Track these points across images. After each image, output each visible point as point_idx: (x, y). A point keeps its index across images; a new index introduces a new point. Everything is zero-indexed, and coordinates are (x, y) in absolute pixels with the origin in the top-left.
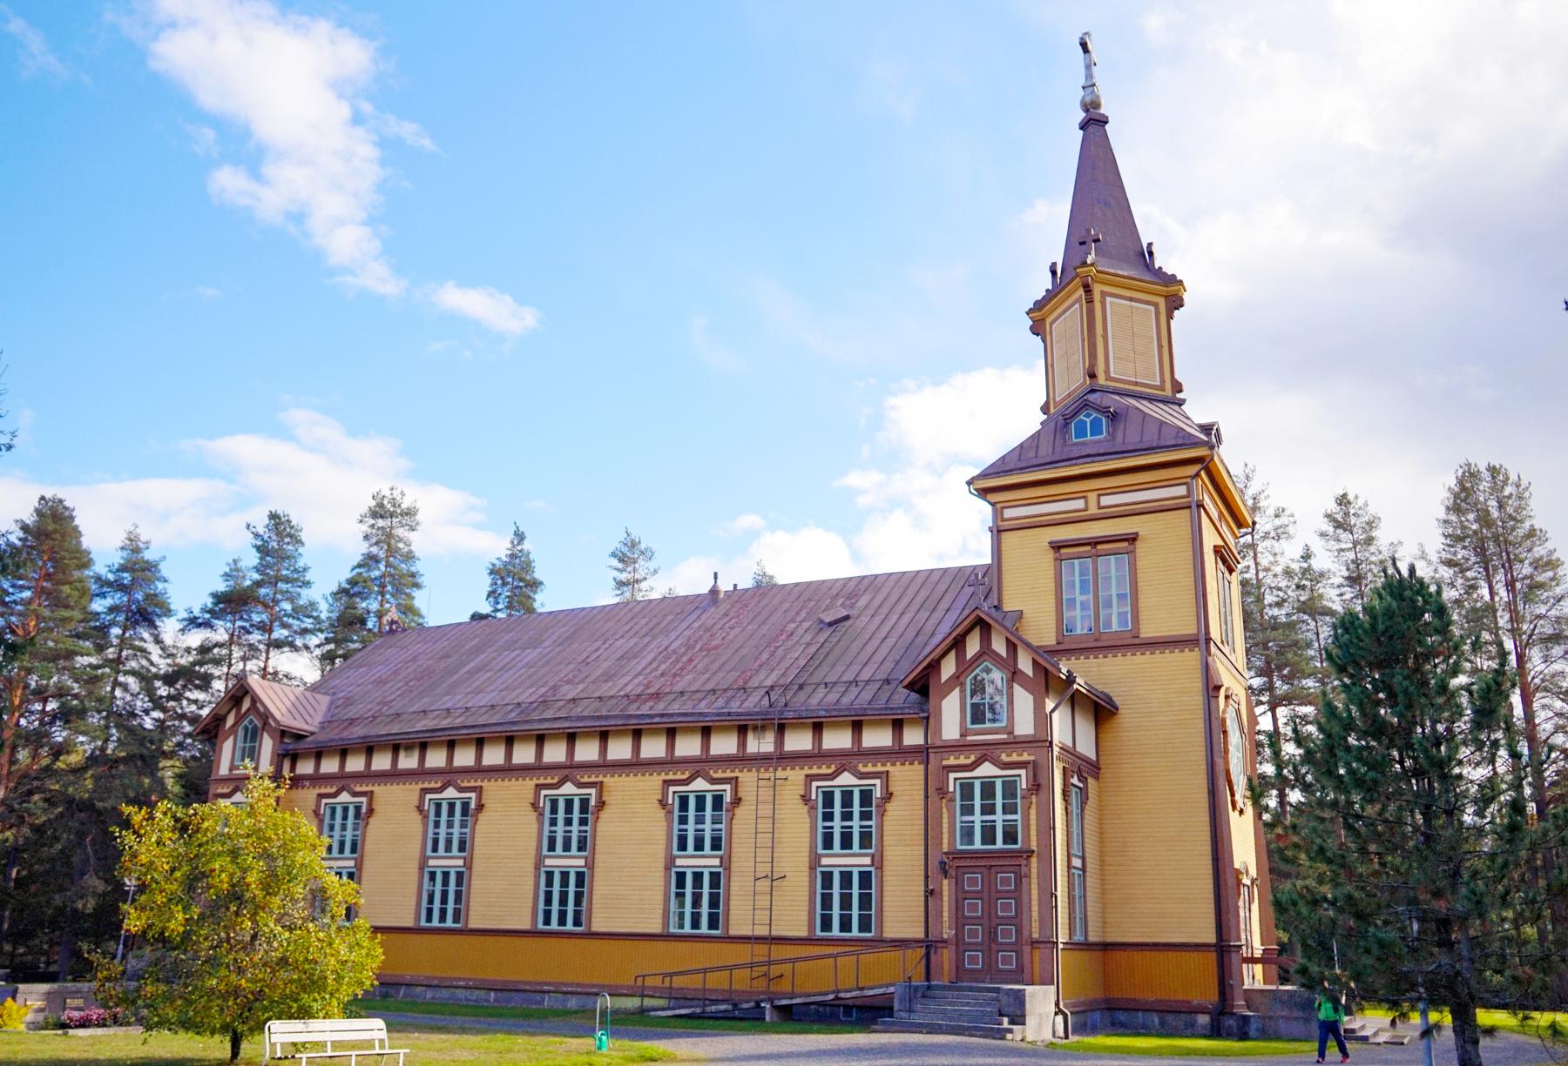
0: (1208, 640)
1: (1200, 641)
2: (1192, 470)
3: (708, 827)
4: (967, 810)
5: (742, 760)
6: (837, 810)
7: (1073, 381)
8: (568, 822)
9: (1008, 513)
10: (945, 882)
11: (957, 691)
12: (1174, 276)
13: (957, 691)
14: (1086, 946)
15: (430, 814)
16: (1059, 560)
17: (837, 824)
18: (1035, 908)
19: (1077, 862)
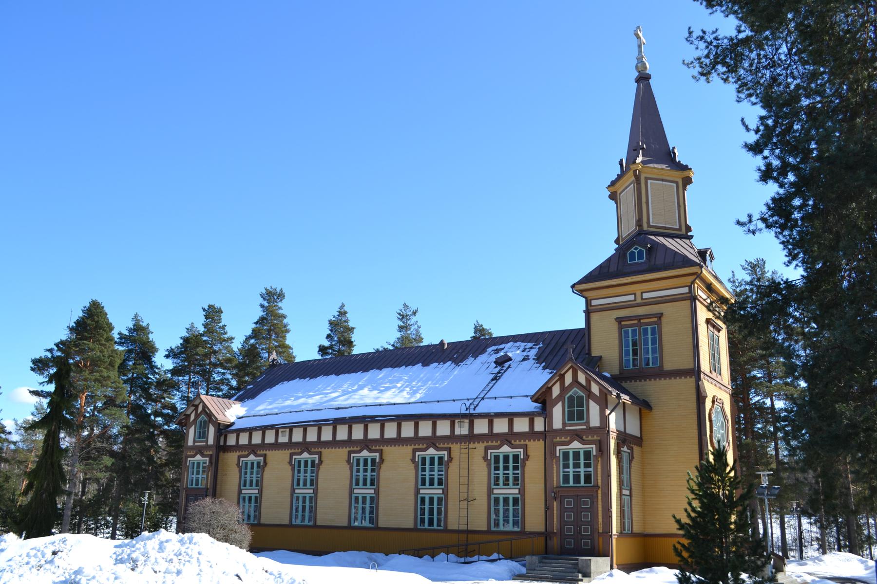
0: (699, 371)
1: (696, 372)
2: (691, 278)
3: (436, 473)
4: (566, 466)
5: (453, 438)
6: (501, 465)
7: (630, 228)
8: (365, 470)
9: (594, 303)
10: (555, 503)
11: (560, 404)
12: (687, 166)
13: (560, 404)
14: (633, 535)
15: (296, 467)
16: (621, 327)
17: (571, 470)
18: (600, 518)
19: (626, 492)
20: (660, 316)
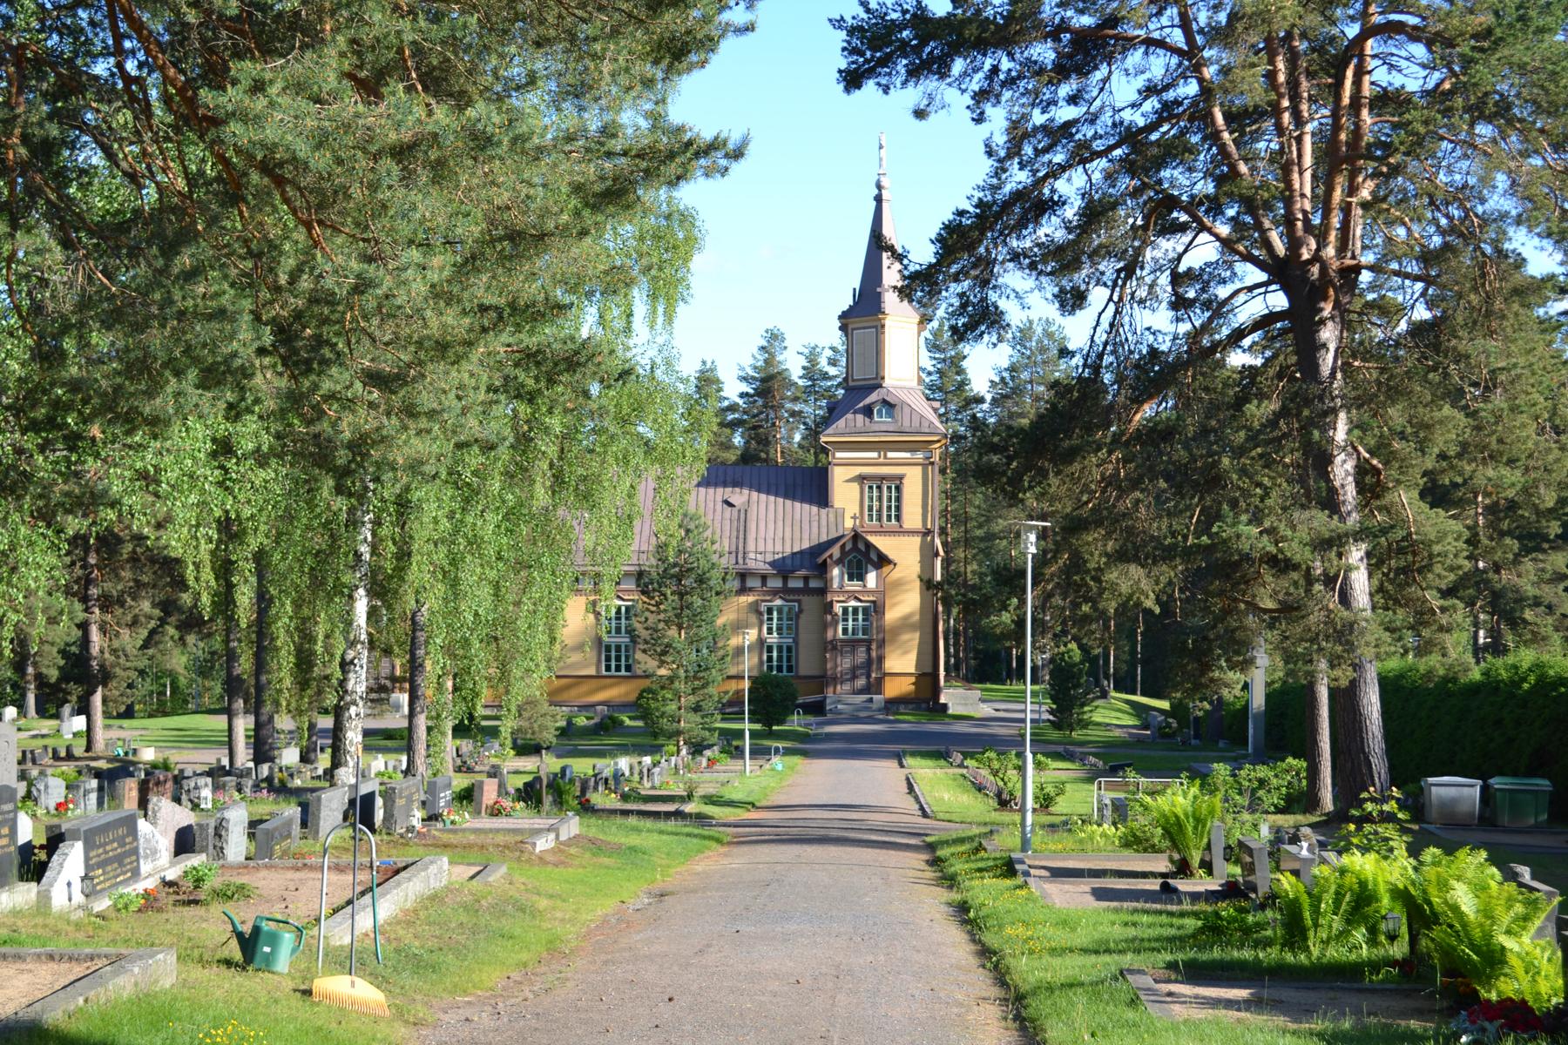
20: (901, 478)
